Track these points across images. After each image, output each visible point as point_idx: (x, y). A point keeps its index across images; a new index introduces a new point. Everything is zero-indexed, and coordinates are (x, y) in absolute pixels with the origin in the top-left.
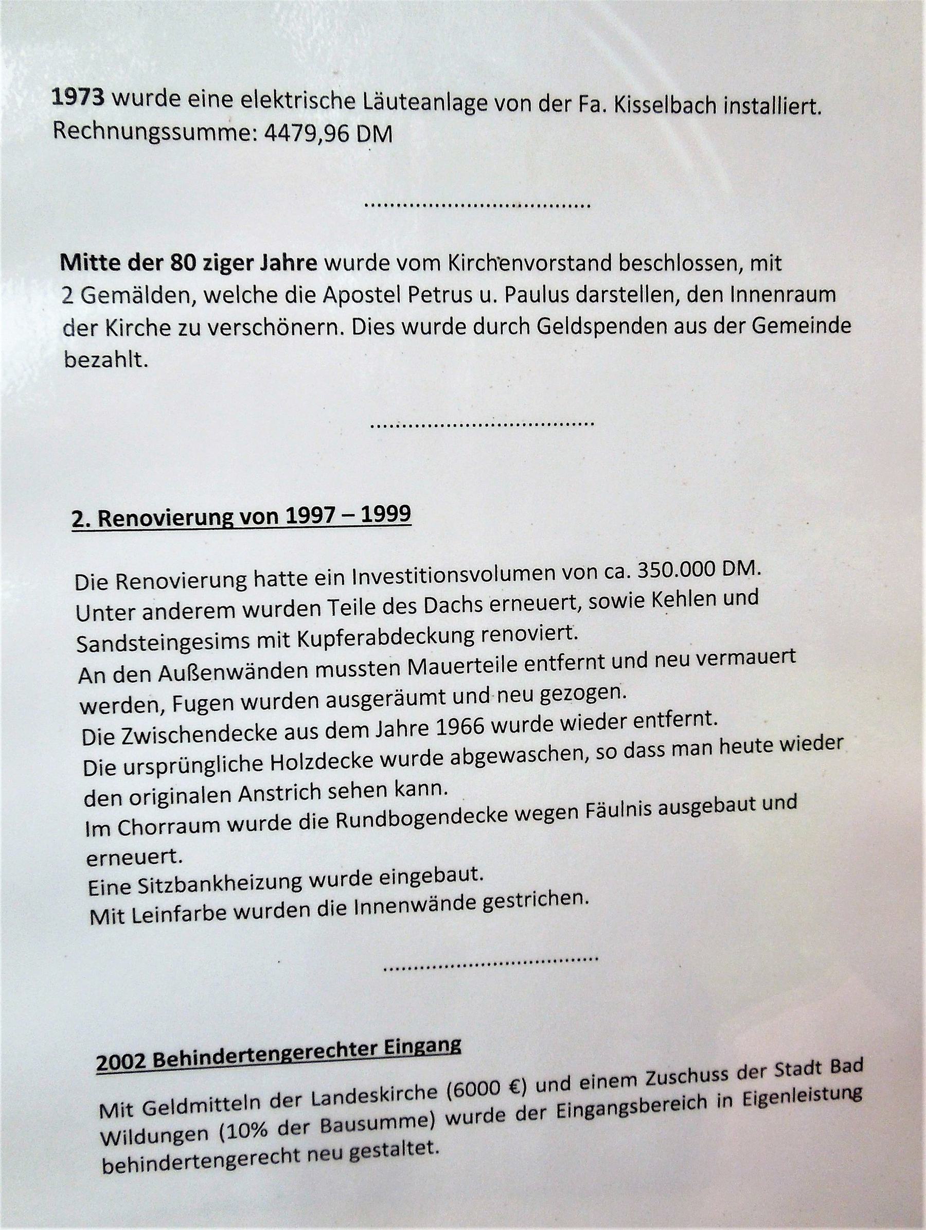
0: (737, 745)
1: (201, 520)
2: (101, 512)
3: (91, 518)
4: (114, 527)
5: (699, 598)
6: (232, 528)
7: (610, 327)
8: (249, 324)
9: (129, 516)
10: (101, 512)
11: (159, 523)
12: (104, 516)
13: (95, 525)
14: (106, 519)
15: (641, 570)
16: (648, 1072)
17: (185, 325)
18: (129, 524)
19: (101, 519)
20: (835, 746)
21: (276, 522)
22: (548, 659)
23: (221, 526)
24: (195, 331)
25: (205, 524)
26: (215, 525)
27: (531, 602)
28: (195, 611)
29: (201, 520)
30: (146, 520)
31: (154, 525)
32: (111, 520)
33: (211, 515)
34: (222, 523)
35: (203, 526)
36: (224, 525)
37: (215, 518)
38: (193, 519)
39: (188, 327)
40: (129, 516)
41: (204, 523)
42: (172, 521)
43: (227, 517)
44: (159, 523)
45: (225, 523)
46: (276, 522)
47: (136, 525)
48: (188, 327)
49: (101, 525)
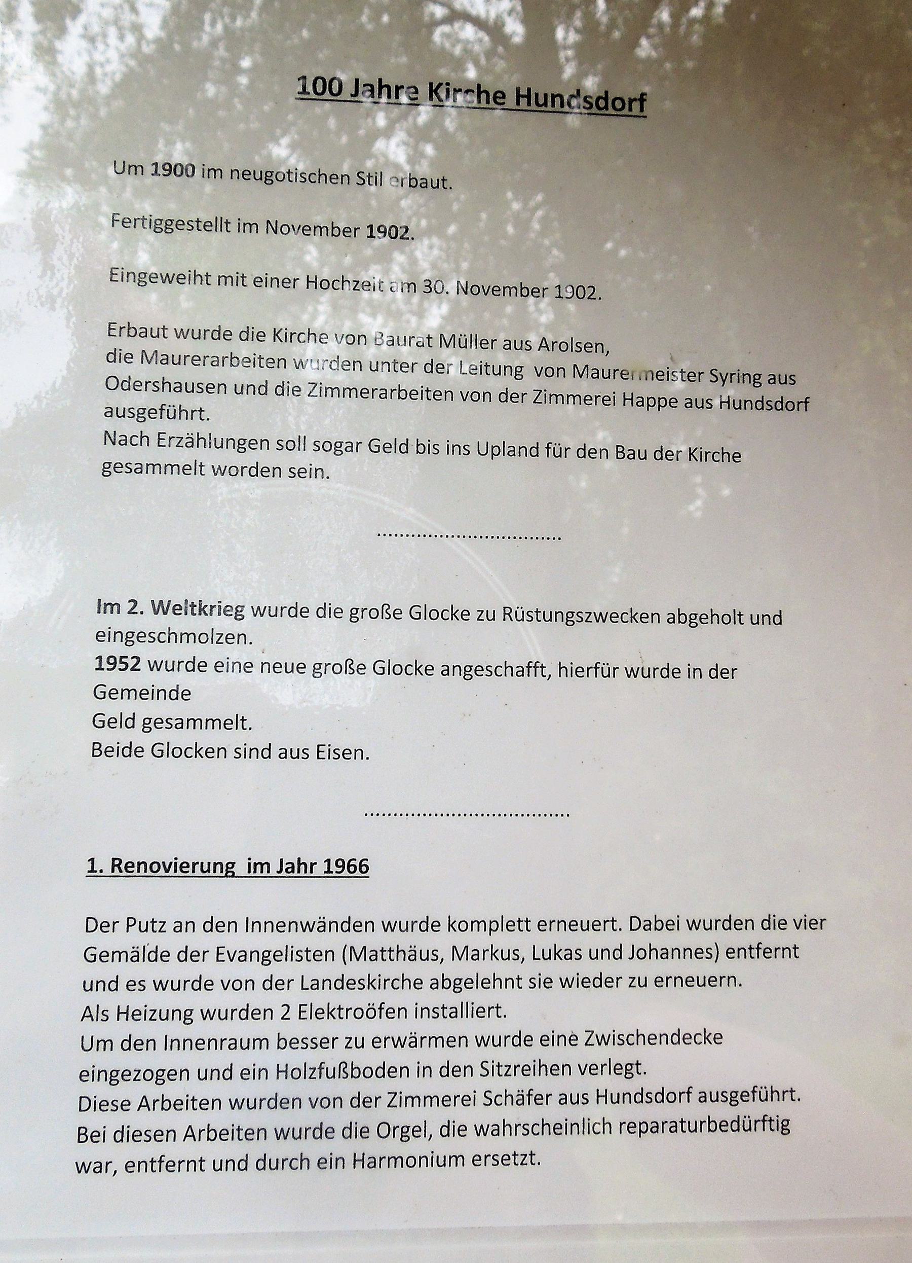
0: (724, 1123)
1: (205, 869)
2: (114, 859)
3: (104, 864)
4: (124, 873)
5: (738, 922)
6: (233, 876)
7: (656, 1128)
8: (339, 750)
9: (139, 864)
10: (114, 859)
11: (167, 871)
12: (116, 863)
13: (107, 871)
14: (118, 865)
15: (426, 286)
16: (630, 978)
17: (634, 978)
18: (139, 871)
19: (113, 866)
20: (224, 669)
21: (268, 872)
22: (148, 1160)
23: (223, 874)
24: (642, 983)
25: (209, 872)
26: (218, 873)
27: (283, 924)
28: (719, 979)
29: (205, 869)
30: (155, 867)
31: (162, 872)
32: (122, 866)
33: (215, 864)
34: (224, 872)
35: (207, 874)
36: (226, 874)
37: (218, 866)
38: (198, 867)
39: (636, 980)
40: (139, 864)
41: (209, 871)
42: (178, 869)
43: (230, 866)
44: (167, 871)
45: (227, 872)
46: (268, 872)
47: (145, 871)
48: (636, 980)
49: (113, 871)
